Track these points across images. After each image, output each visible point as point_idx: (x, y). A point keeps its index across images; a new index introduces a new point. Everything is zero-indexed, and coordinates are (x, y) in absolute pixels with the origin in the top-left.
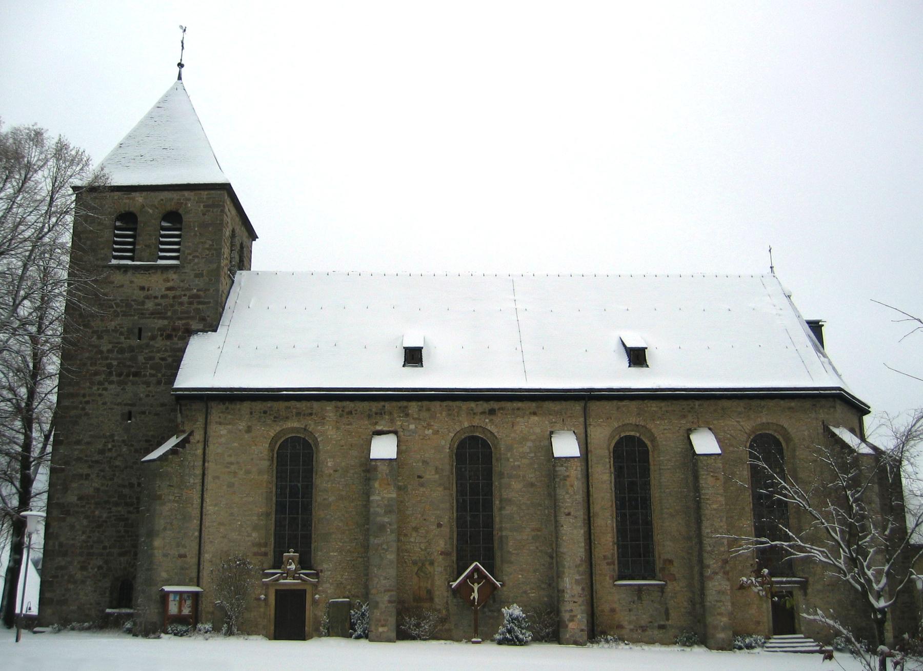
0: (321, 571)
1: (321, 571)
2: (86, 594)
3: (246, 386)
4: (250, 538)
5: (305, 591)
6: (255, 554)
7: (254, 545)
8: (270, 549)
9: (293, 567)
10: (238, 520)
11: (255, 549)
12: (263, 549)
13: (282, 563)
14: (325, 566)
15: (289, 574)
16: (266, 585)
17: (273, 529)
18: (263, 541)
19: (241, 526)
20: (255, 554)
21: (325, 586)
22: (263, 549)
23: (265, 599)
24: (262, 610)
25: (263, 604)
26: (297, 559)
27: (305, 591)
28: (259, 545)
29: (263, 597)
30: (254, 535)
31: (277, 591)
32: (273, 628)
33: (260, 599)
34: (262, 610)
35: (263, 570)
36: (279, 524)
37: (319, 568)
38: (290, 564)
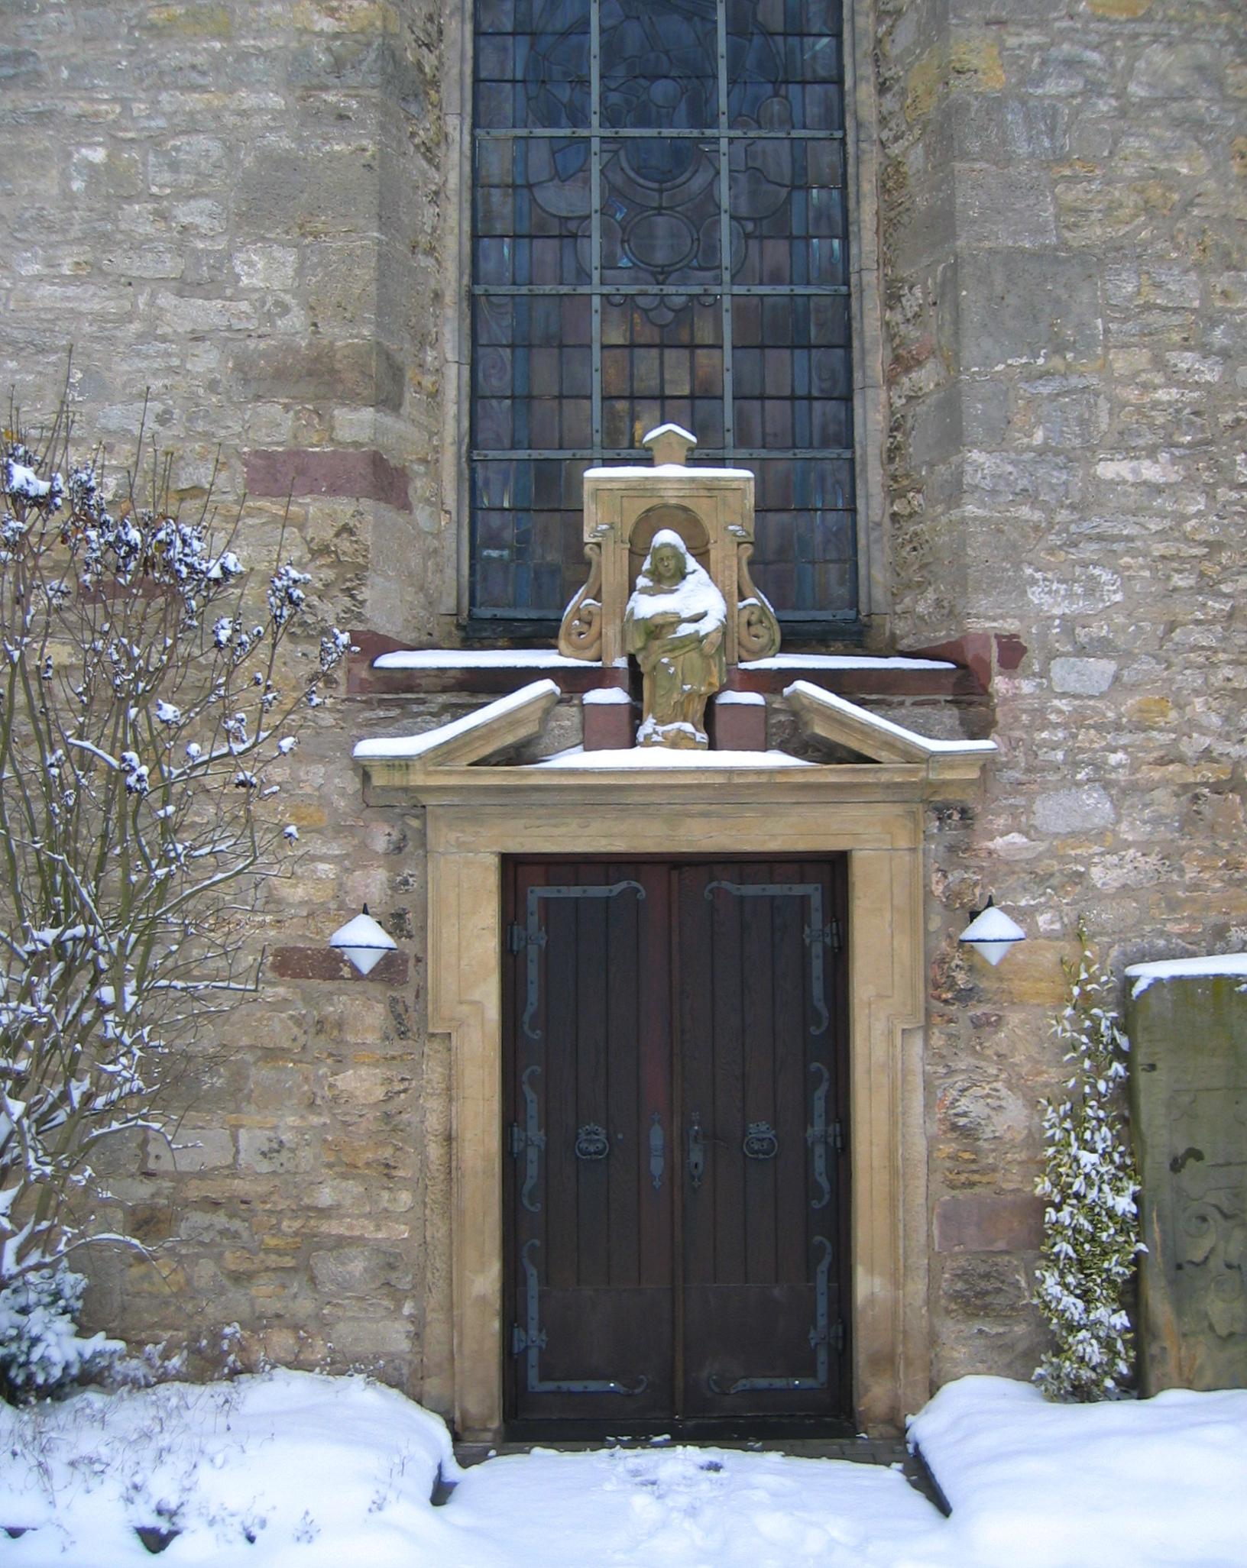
0: (1012, 653)
1: (1012, 653)
2: (553, 641)
3: (496, 1106)
4: (205, 312)
5: (832, 869)
6: (276, 474)
7: (267, 375)
8: (432, 430)
9: (700, 600)
10: (85, 125)
11: (275, 424)
12: (356, 424)
13: (578, 565)
14: (1048, 599)
15: (640, 683)
16: (400, 807)
17: (454, 244)
18: (350, 337)
19: (115, 186)
20: (276, 474)
21: (1054, 812)
22: (356, 424)
23: (390, 967)
24: (361, 1083)
25: (367, 1016)
26: (732, 526)
27: (832, 869)
28: (316, 377)
29: (364, 937)
30: (263, 268)
31: (515, 869)
32: (485, 1281)
33: (331, 963)
34: (361, 1083)
35: (374, 644)
36: (508, 219)
37: (987, 619)
38: (669, 576)
